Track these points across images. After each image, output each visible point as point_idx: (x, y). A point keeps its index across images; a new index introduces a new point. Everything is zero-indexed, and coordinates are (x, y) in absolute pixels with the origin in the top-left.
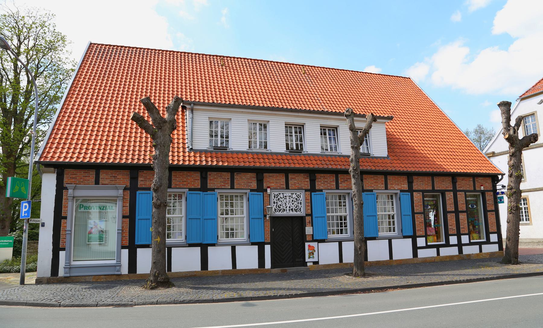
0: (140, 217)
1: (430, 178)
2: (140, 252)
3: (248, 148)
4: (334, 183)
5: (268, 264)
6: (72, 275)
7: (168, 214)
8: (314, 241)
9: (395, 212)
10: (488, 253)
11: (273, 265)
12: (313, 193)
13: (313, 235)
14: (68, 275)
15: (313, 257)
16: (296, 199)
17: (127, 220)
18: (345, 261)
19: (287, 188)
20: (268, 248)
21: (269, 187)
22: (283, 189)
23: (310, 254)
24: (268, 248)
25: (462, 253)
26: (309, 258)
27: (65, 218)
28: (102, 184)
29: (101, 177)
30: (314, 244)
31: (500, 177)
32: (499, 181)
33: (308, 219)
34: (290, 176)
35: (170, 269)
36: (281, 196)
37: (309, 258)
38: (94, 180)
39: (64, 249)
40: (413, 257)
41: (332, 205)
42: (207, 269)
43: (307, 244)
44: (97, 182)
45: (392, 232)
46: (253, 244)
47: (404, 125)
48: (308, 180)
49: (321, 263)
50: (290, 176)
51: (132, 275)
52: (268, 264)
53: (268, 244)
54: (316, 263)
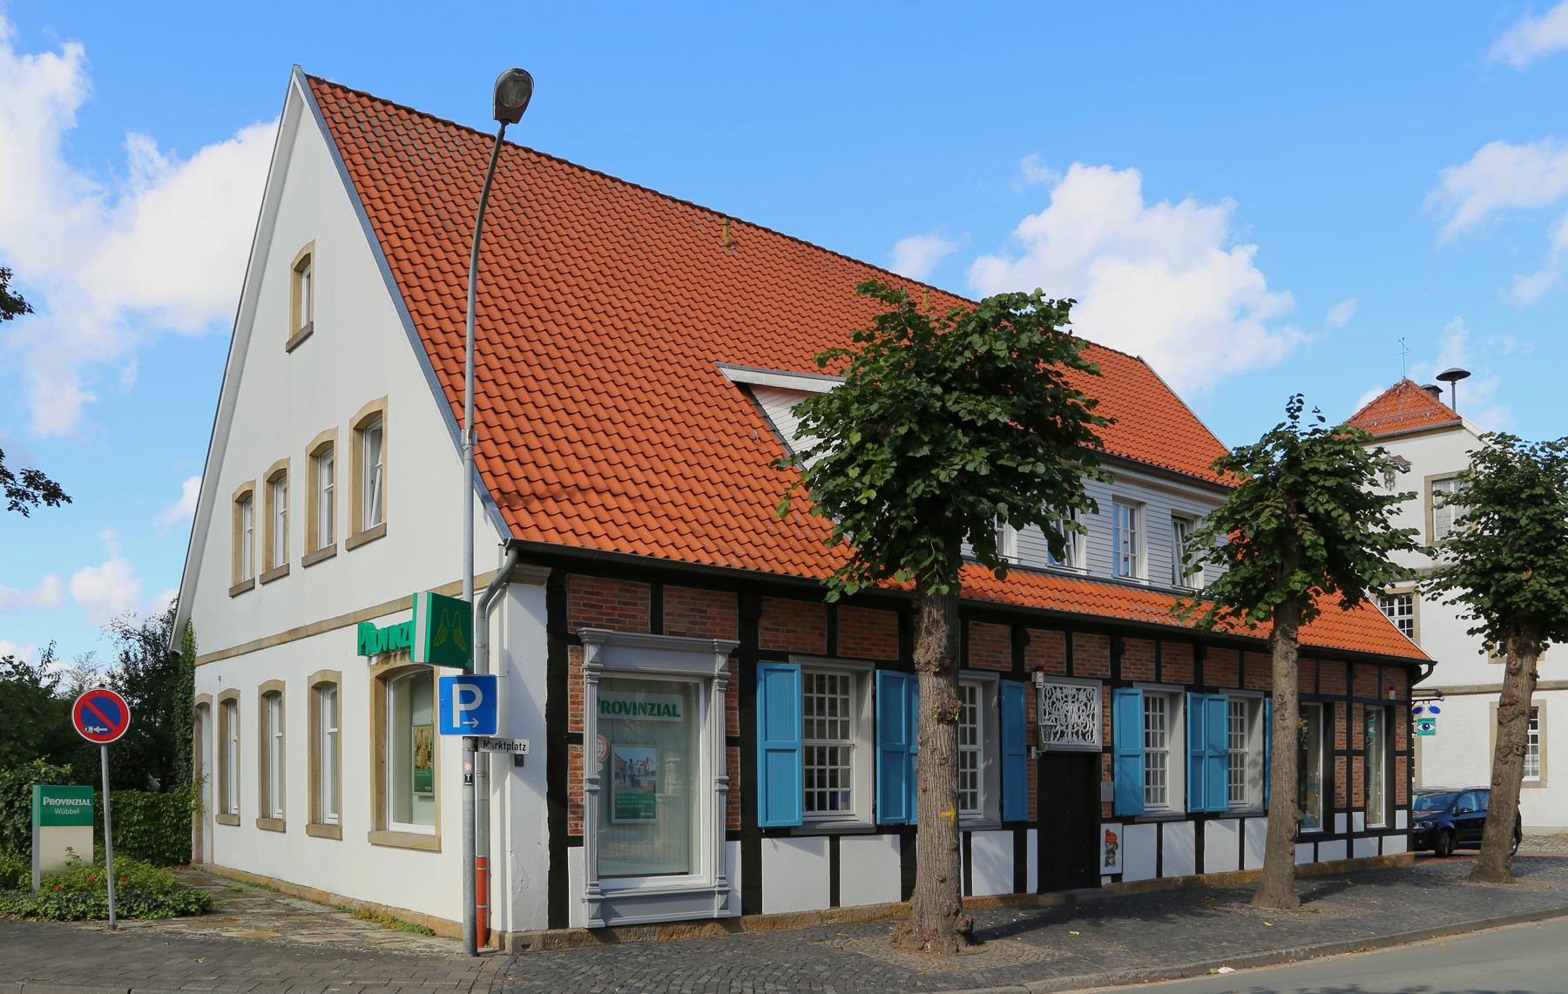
0: (774, 743)
2: (1344, 831)
4: (1153, 666)
5: (1032, 885)
6: (614, 921)
8: (1115, 819)
12: (1118, 691)
13: (1113, 804)
14: (600, 923)
15: (1114, 864)
18: (1210, 868)
19: (1070, 674)
20: (1032, 835)
21: (1039, 668)
22: (1058, 674)
23: (1108, 852)
24: (1032, 835)
26: (1107, 864)
27: (578, 739)
28: (671, 633)
29: (666, 608)
30: (1115, 828)
31: (1424, 668)
32: (1421, 678)
34: (1077, 639)
35: (968, 891)
36: (1058, 694)
37: (1107, 864)
38: (647, 618)
39: (578, 842)
42: (760, 912)
43: (1104, 827)
44: (657, 628)
46: (1006, 826)
47: (614, 458)
48: (1107, 653)
52: (1032, 885)
53: (1032, 826)
54: (1117, 878)
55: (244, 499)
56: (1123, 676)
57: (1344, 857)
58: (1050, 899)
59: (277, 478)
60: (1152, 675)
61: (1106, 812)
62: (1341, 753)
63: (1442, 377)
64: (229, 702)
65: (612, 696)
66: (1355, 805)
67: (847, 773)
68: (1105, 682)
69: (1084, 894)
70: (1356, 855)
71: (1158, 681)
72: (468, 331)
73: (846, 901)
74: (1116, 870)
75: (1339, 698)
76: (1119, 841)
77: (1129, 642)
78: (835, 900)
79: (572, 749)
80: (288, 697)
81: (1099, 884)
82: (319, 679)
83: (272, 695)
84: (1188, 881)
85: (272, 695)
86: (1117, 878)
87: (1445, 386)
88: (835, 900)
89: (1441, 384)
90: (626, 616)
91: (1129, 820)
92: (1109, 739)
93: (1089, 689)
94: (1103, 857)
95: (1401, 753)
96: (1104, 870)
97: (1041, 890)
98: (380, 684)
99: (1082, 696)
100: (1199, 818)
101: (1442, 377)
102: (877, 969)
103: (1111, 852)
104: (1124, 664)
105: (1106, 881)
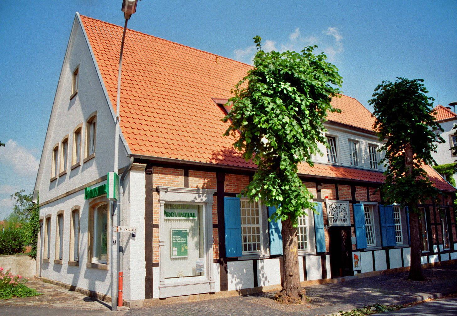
1: (333, 186)
2: (440, 245)
3: (350, 164)
4: (366, 195)
7: (245, 223)
8: (357, 250)
9: (401, 224)
10: (380, 271)
11: (333, 276)
12: (355, 205)
15: (358, 266)
16: (344, 210)
17: (217, 229)
20: (328, 257)
24: (328, 257)
25: (257, 286)
26: (355, 267)
27: (214, 226)
30: (357, 253)
33: (352, 229)
34: (339, 187)
37: (355, 267)
40: (255, 286)
41: (249, 215)
43: (353, 253)
45: (252, 251)
48: (350, 191)
49: (362, 272)
50: (357, 188)
51: (224, 292)
52: (329, 276)
54: (359, 272)
55: (56, 150)
56: (356, 199)
57: (448, 259)
58: (336, 281)
59: (65, 142)
60: (366, 199)
61: (354, 248)
62: (433, 224)
63: (450, 105)
64: (48, 219)
65: (169, 211)
66: (440, 242)
67: (73, 190)
68: (350, 202)
69: (348, 278)
70: (442, 260)
71: (368, 200)
72: (120, 83)
73: (377, 270)
74: (359, 269)
75: (430, 205)
76: (359, 258)
77: (357, 188)
78: (374, 269)
79: (155, 230)
80: (65, 216)
81: (353, 275)
82: (74, 209)
83: (60, 216)
84: (385, 272)
85: (60, 216)
86: (359, 272)
87: (452, 107)
88: (374, 269)
89: (450, 107)
90: (175, 181)
91: (362, 250)
92: (353, 221)
93: (344, 204)
94: (354, 263)
95: (453, 224)
96: (354, 269)
97: (332, 277)
98: (92, 209)
99: (342, 207)
100: (387, 249)
101: (450, 105)
102: (268, 311)
103: (357, 262)
104: (356, 195)
105: (355, 273)
